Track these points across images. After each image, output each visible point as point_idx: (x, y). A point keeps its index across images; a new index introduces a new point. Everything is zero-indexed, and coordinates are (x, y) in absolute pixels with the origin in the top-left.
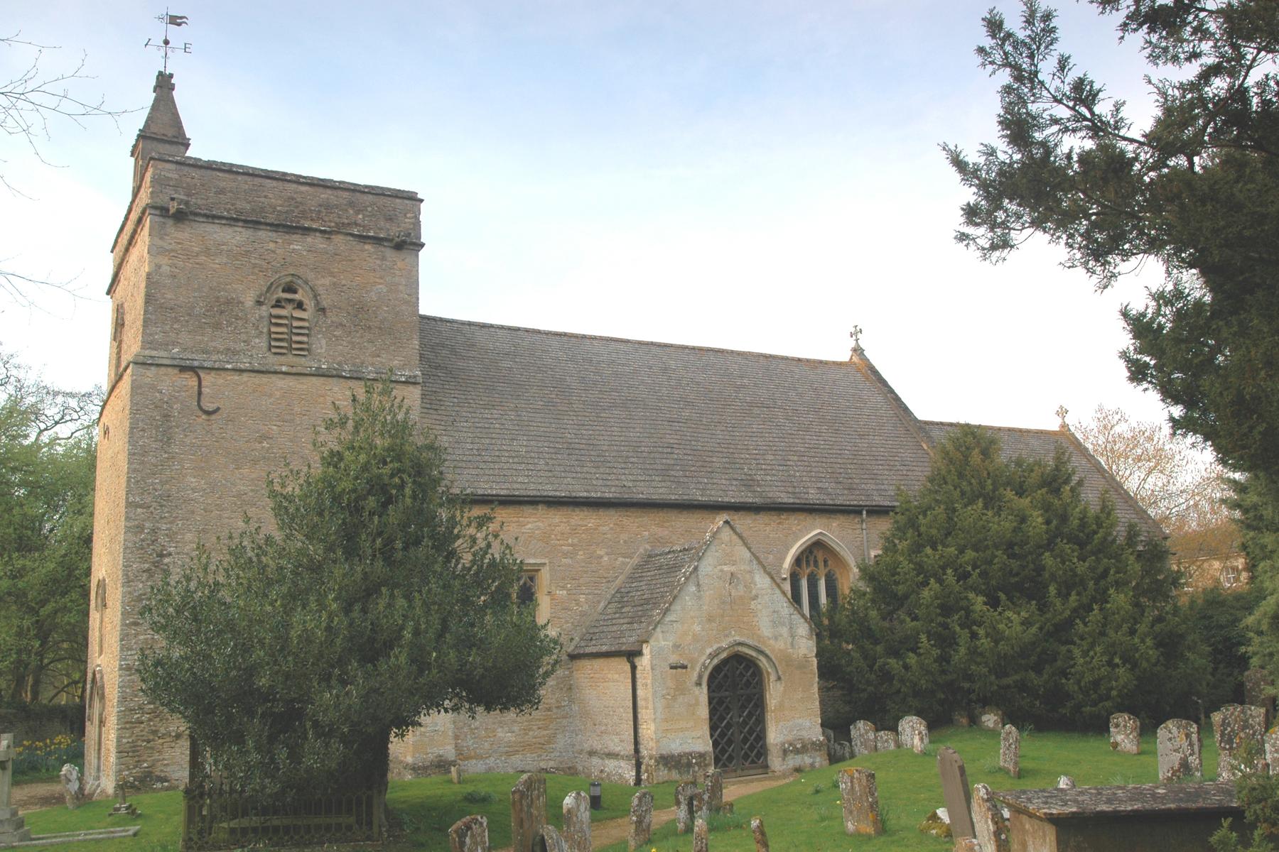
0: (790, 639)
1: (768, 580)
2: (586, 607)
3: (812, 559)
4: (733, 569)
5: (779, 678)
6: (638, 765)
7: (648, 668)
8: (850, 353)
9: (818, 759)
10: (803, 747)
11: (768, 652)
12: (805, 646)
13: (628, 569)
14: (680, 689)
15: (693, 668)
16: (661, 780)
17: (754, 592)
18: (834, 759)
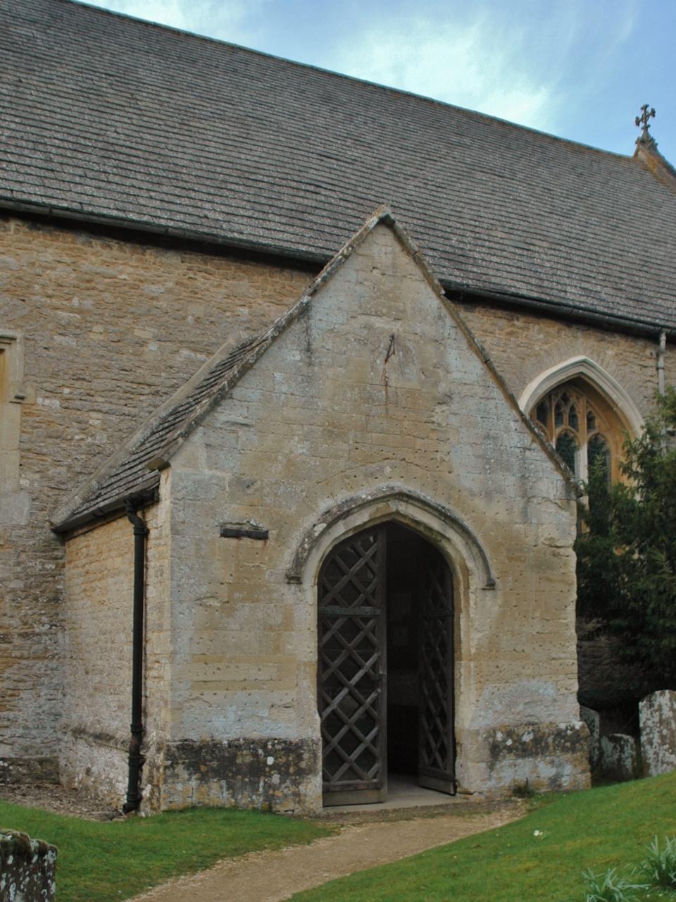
0: (520, 503)
1: (476, 366)
2: (101, 438)
3: (566, 411)
4: (396, 327)
5: (491, 585)
6: (136, 763)
7: (167, 531)
8: (635, 147)
9: (568, 769)
10: (536, 741)
11: (467, 523)
12: (557, 525)
13: (201, 374)
14: (245, 587)
15: (282, 540)
16: (178, 801)
17: (443, 387)
18: (605, 773)
